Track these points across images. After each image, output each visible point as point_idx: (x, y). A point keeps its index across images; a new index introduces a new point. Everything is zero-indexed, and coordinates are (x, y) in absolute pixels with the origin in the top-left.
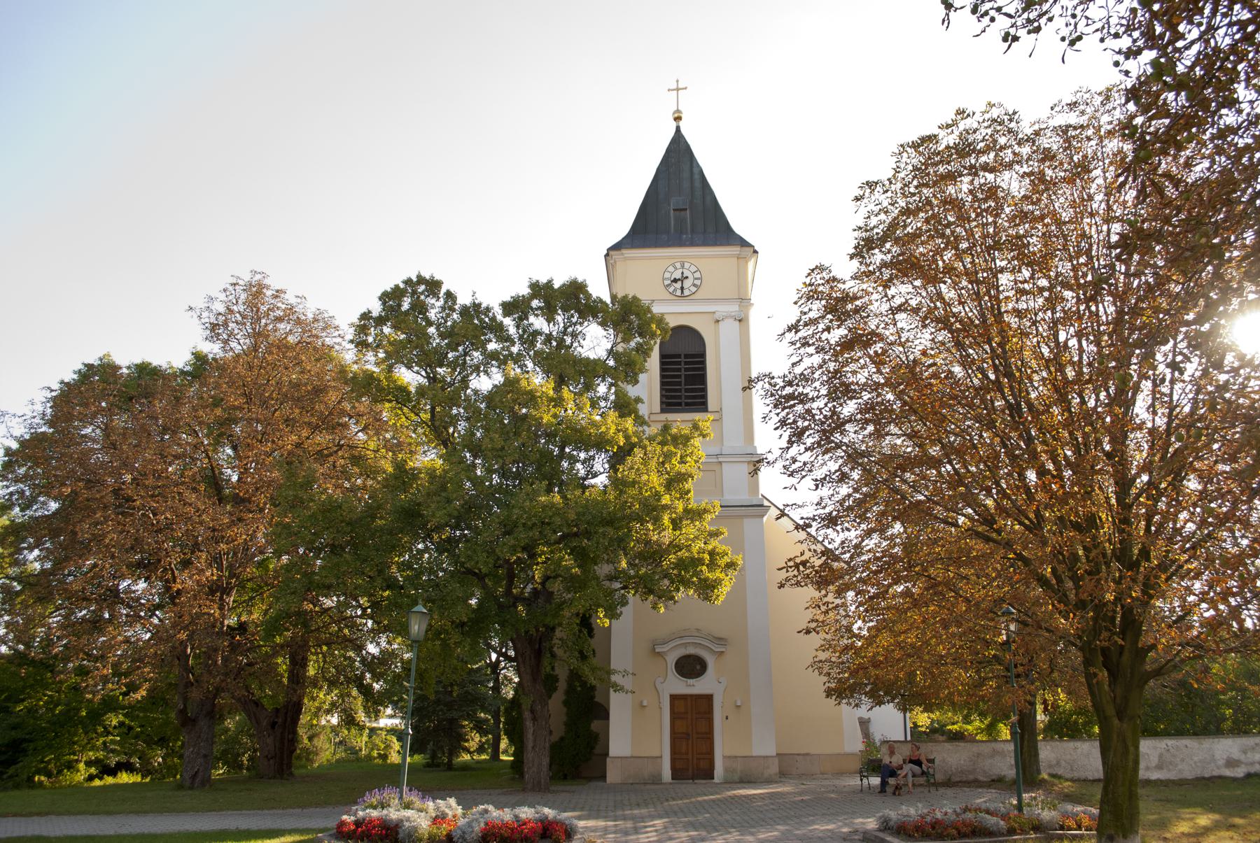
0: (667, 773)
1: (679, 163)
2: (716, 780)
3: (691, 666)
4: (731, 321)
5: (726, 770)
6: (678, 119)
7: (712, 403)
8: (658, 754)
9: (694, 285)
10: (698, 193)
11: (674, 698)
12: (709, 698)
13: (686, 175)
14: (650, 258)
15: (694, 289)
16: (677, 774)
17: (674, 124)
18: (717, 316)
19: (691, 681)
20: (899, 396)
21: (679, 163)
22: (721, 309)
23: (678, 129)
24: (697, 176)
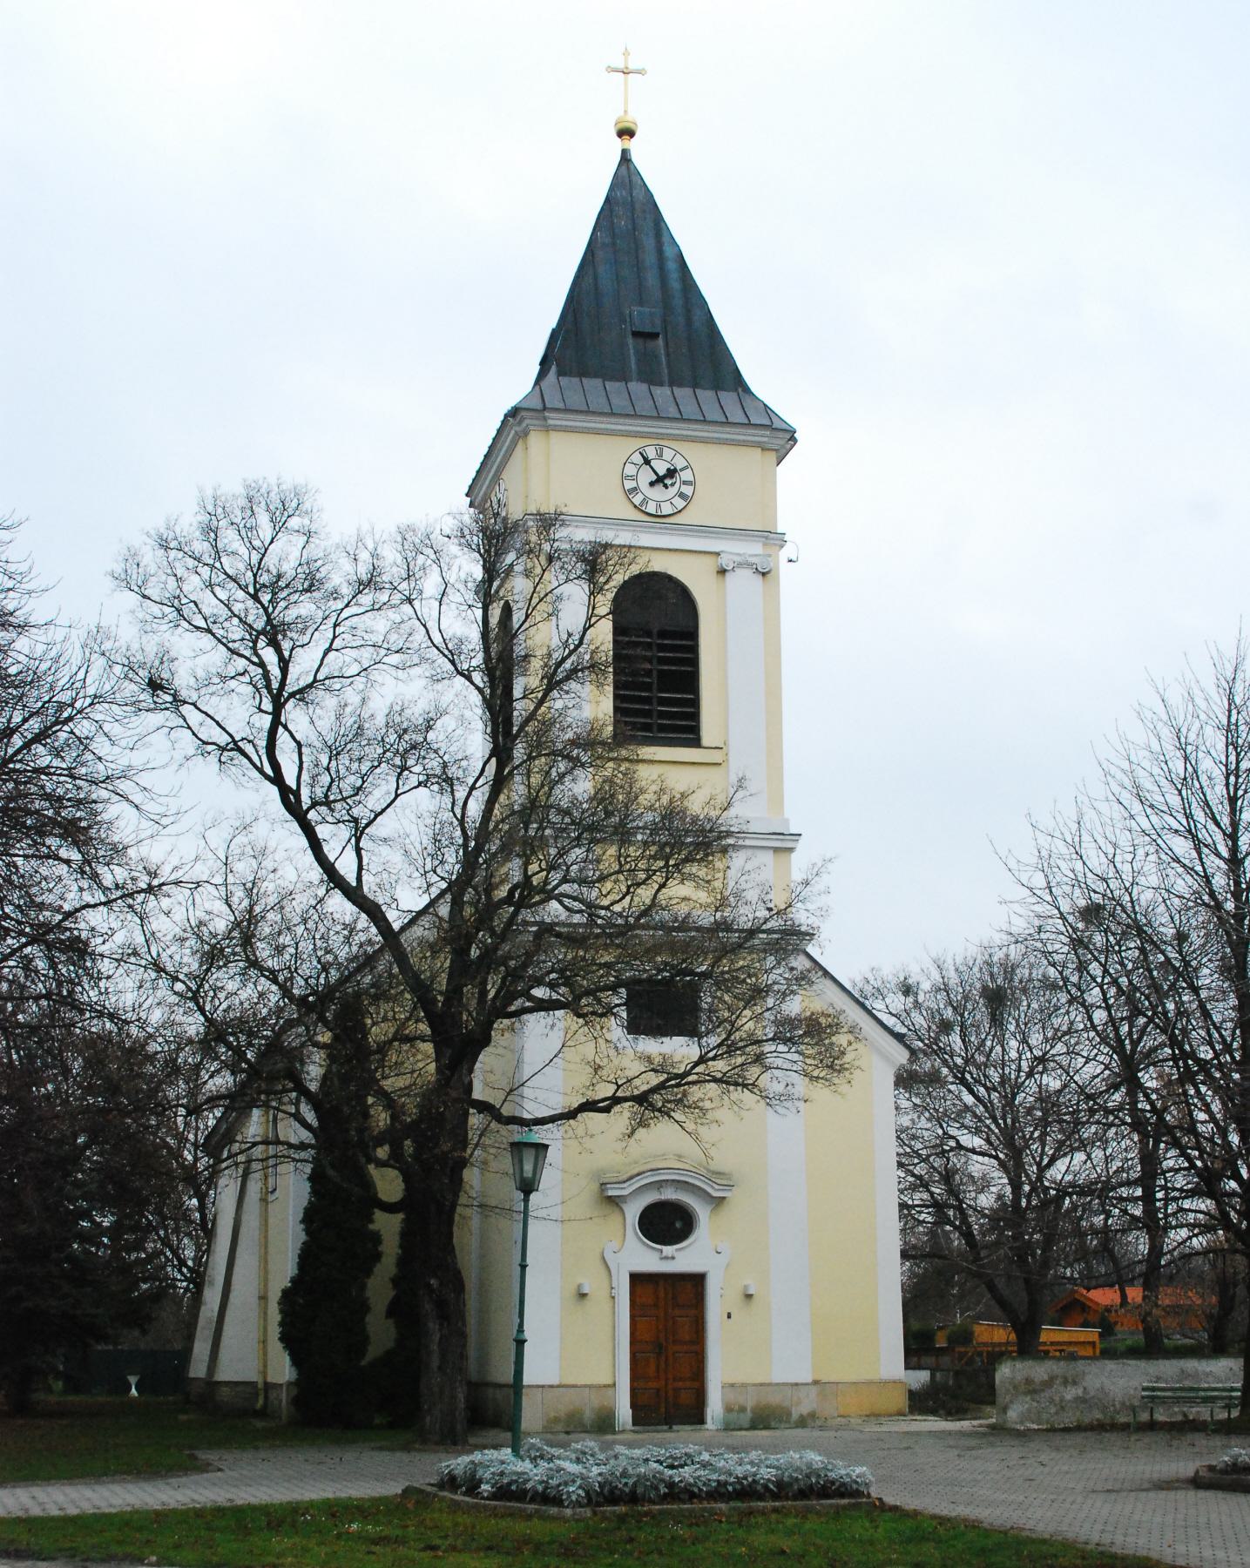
0: (624, 1412)
1: (629, 229)
2: (710, 1425)
3: (666, 1223)
4: (747, 573)
5: (728, 1409)
6: (626, 133)
7: (708, 733)
8: (610, 1382)
9: (682, 496)
10: (678, 302)
11: (637, 1279)
12: (695, 1283)
13: (650, 258)
14: (566, 429)
15: (680, 503)
16: (637, 1421)
17: (617, 145)
18: (725, 561)
19: (668, 1250)
20: (48, 1096)
21: (629, 229)
22: (732, 549)
23: (625, 158)
24: (672, 266)
